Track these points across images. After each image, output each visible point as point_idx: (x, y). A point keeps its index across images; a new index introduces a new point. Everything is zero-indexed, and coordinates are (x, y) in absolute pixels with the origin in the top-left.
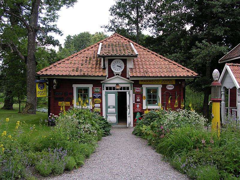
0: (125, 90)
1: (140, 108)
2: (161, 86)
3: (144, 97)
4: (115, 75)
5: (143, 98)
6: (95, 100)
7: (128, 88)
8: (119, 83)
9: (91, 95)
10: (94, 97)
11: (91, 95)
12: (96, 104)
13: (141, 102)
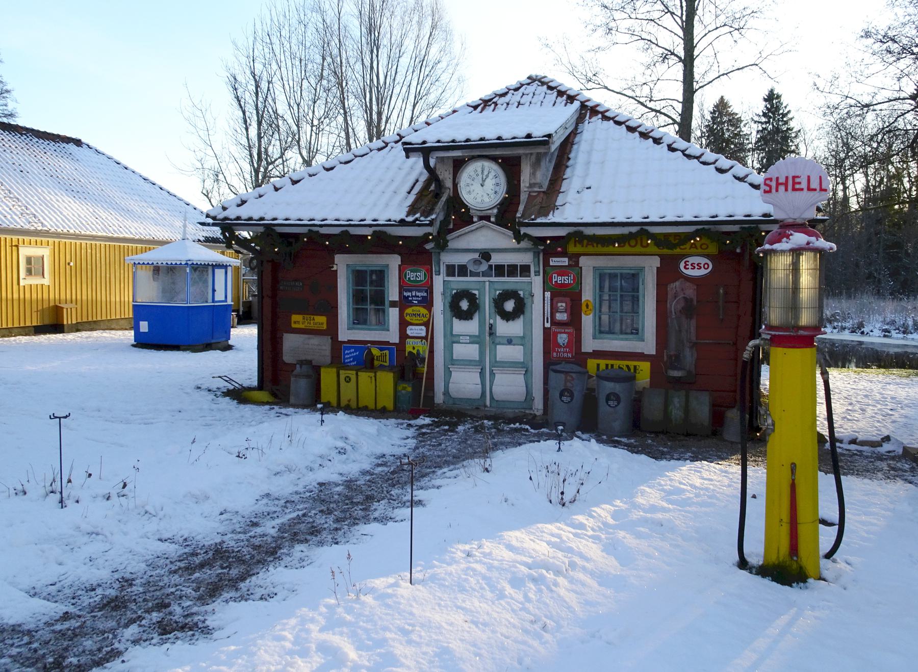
0: (454, 276)
1: (569, 345)
2: (656, 262)
3: (587, 306)
4: (475, 219)
5: (584, 308)
6: (409, 311)
7: (525, 270)
8: (494, 250)
9: (393, 294)
10: (403, 303)
11: (393, 294)
12: (410, 327)
13: (575, 322)
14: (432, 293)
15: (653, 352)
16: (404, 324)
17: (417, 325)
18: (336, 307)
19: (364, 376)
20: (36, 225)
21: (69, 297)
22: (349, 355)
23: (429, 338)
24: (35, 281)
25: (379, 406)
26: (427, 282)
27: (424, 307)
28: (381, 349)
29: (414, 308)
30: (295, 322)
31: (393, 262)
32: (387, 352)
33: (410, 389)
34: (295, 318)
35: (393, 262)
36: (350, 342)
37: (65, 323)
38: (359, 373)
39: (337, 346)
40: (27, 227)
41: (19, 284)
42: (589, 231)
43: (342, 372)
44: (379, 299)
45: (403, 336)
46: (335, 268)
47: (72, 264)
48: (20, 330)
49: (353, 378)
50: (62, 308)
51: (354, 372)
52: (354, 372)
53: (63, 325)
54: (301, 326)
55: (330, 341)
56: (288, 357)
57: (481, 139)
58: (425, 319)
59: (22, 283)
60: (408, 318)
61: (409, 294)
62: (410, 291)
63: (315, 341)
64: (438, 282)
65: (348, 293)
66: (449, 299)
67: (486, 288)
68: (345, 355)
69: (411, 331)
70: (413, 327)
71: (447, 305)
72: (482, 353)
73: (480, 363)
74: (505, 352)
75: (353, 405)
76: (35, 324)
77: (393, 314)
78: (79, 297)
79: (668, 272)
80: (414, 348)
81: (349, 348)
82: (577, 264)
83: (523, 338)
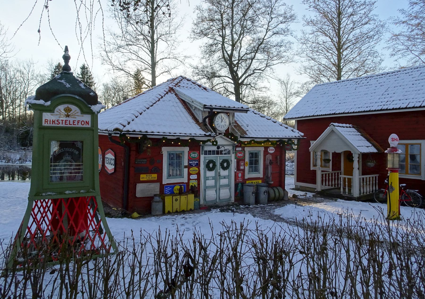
6: (191, 169)
10: (189, 166)
14: (200, 161)
15: (262, 177)
16: (189, 174)
19: (183, 198)
22: (167, 190)
23: (198, 179)
25: (189, 209)
30: (142, 178)
31: (186, 149)
35: (186, 149)
36: (168, 184)
42: (256, 140)
43: (174, 197)
44: (179, 164)
45: (189, 179)
54: (145, 179)
57: (229, 107)
58: (197, 172)
60: (191, 172)
62: (192, 161)
63: (152, 185)
64: (202, 157)
67: (218, 159)
72: (216, 183)
73: (215, 186)
74: (224, 182)
75: (178, 210)
79: (266, 152)
81: (167, 187)
82: (244, 150)
83: (229, 176)
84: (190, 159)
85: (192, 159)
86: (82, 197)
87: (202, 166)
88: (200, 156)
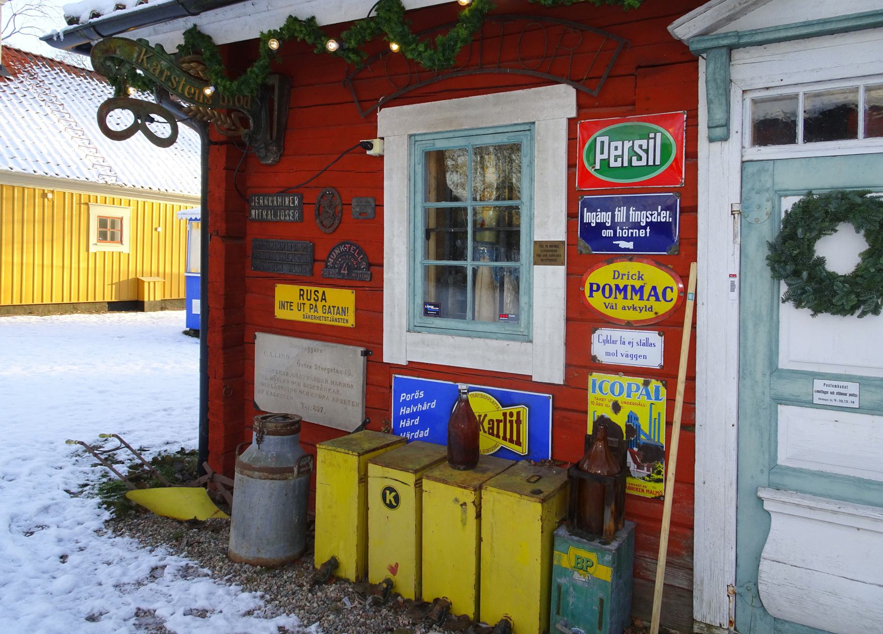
6: (602, 275)
9: (547, 218)
10: (587, 246)
11: (547, 218)
12: (603, 333)
14: (691, 209)
16: (581, 321)
17: (629, 325)
18: (376, 265)
19: (444, 499)
20: (107, 179)
21: (154, 269)
22: (410, 404)
23: (674, 374)
24: (109, 247)
26: (675, 168)
27: (659, 263)
28: (505, 401)
29: (622, 266)
30: (282, 306)
32: (524, 411)
33: (604, 573)
34: (284, 293)
36: (414, 368)
37: (146, 299)
38: (426, 484)
39: (379, 376)
40: (93, 178)
41: (88, 250)
45: (580, 361)
46: (374, 151)
47: (159, 229)
48: (88, 306)
49: (407, 495)
50: (143, 282)
51: (410, 478)
52: (410, 478)
53: (143, 302)
54: (295, 315)
55: (361, 360)
56: (266, 397)
58: (663, 307)
59: (92, 249)
60: (597, 301)
61: (604, 217)
64: (721, 169)
65: (412, 220)
66: (767, 230)
68: (398, 406)
69: (605, 345)
70: (616, 334)
71: (759, 256)
76: (108, 299)
77: (547, 285)
78: (168, 270)
80: (616, 408)
81: (410, 388)
84: (582, 187)
85: (613, 188)
86: (668, 555)
87: (722, 250)
88: (692, 155)
